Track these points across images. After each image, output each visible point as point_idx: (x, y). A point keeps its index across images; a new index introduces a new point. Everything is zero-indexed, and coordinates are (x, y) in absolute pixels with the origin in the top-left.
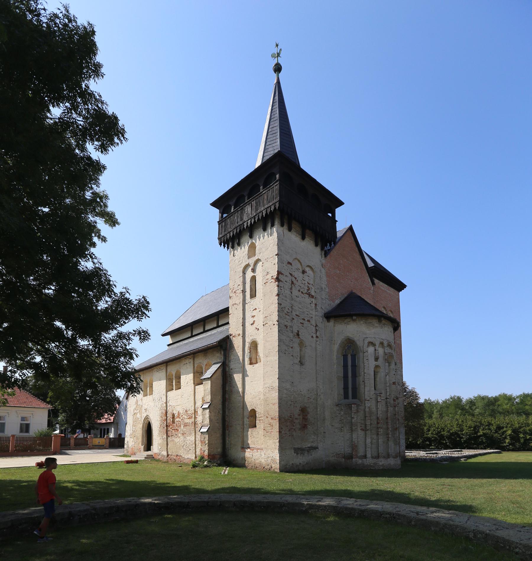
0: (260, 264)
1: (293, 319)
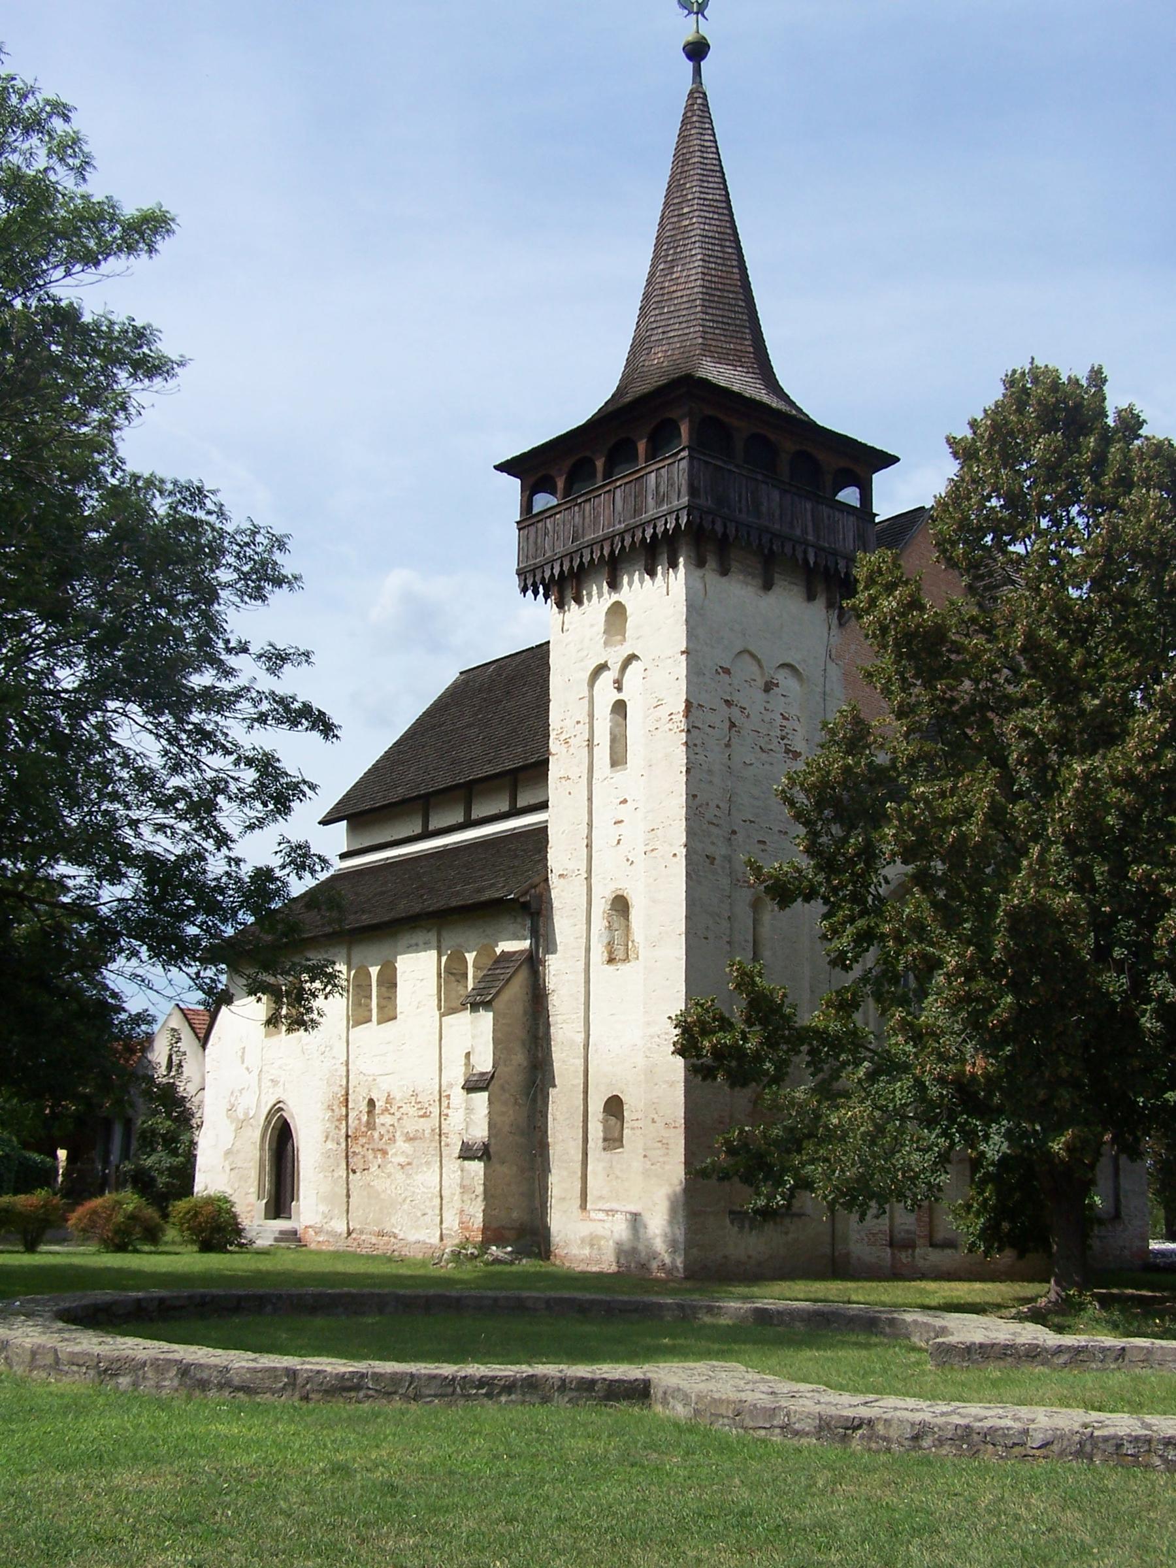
0: (634, 666)
1: (734, 832)
